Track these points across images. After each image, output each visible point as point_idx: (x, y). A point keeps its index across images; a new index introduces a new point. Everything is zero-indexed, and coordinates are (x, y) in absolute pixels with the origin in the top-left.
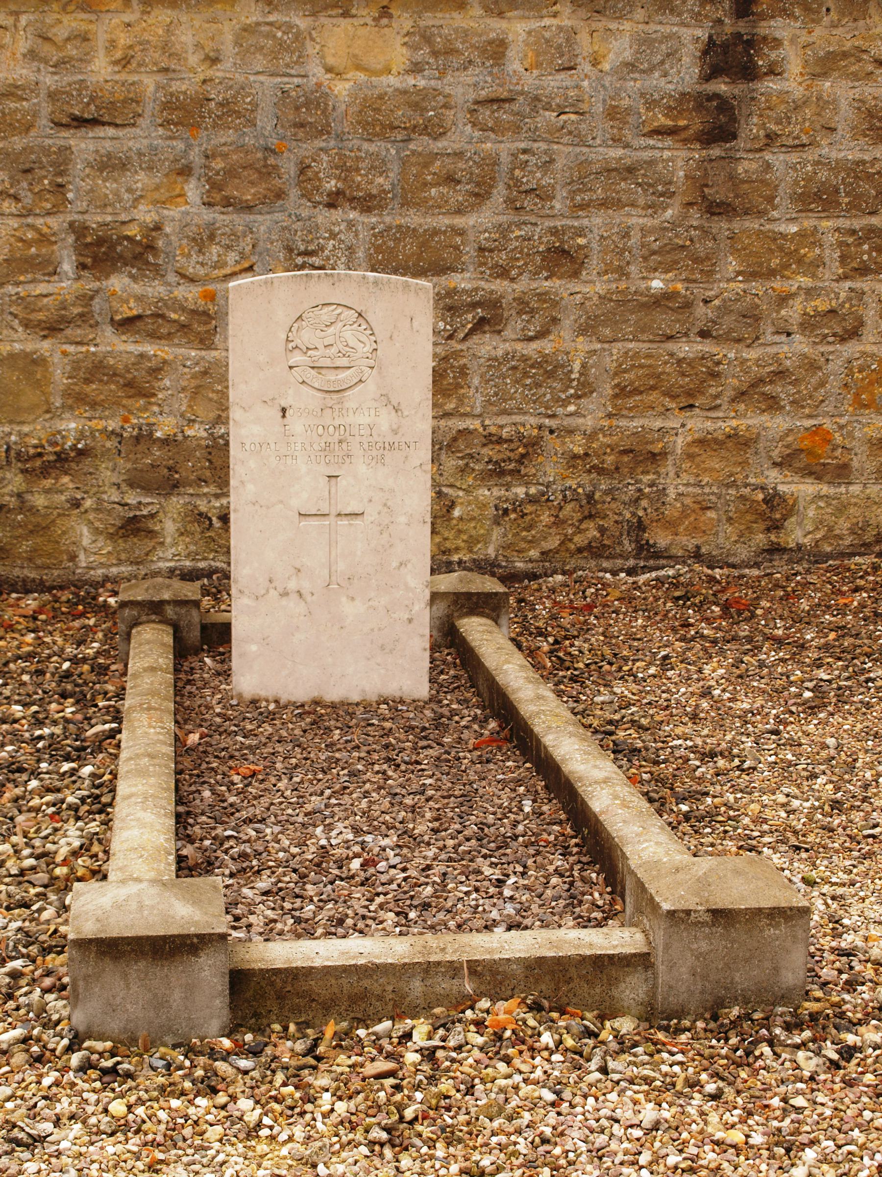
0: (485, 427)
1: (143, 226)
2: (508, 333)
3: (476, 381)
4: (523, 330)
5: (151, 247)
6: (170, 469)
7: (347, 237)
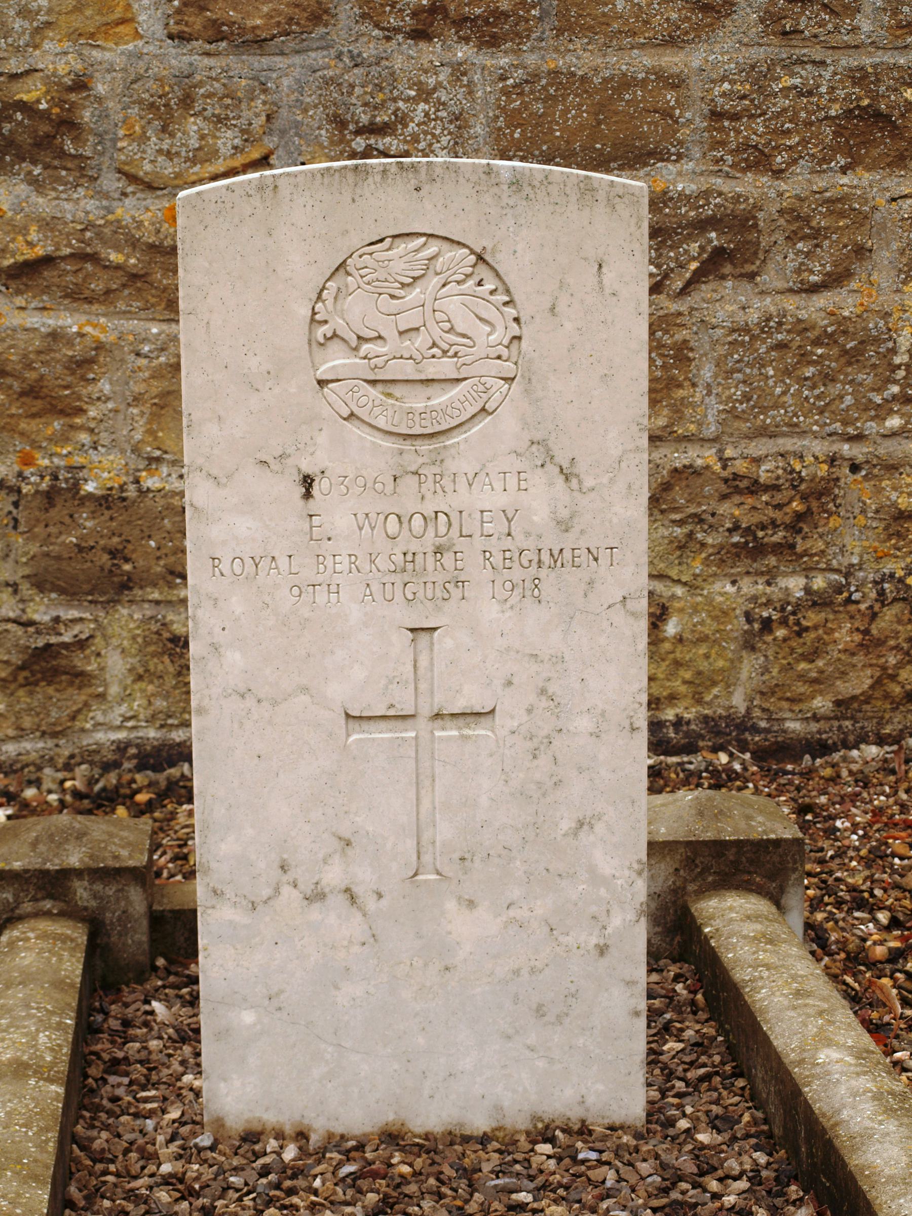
0: (725, 462)
1: (53, 81)
2: (769, 278)
3: (707, 373)
4: (798, 271)
5: (68, 124)
6: (113, 553)
7: (453, 97)
